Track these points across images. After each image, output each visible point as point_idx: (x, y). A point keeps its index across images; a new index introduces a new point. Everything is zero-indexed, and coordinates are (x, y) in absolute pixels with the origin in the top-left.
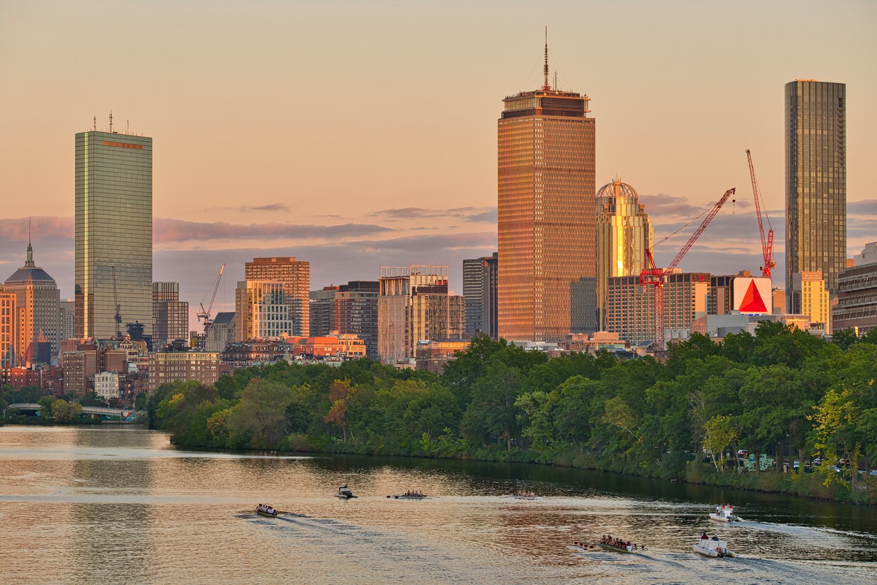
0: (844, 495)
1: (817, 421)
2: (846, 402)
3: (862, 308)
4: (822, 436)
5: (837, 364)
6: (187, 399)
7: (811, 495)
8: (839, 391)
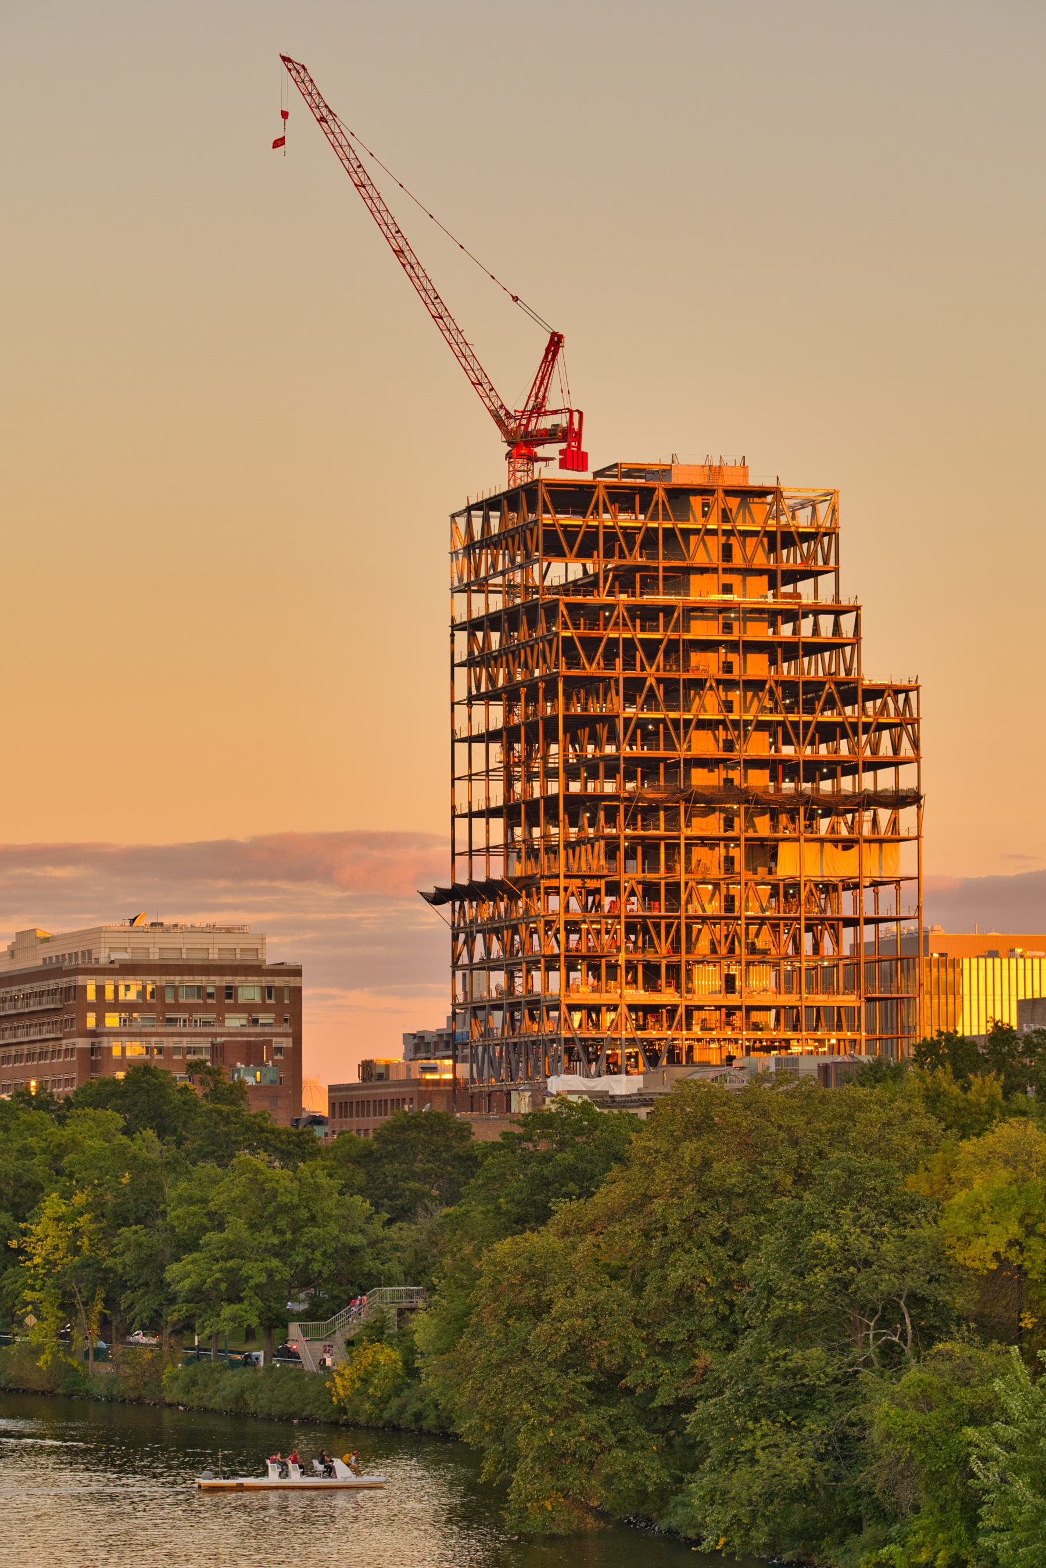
0: (74, 1384)
1: (28, 1249)
2: (81, 1214)
3: (34, 1045)
4: (35, 1277)
5: (49, 1147)
6: (286, 1327)
7: (11, 1385)
8: (67, 1195)
